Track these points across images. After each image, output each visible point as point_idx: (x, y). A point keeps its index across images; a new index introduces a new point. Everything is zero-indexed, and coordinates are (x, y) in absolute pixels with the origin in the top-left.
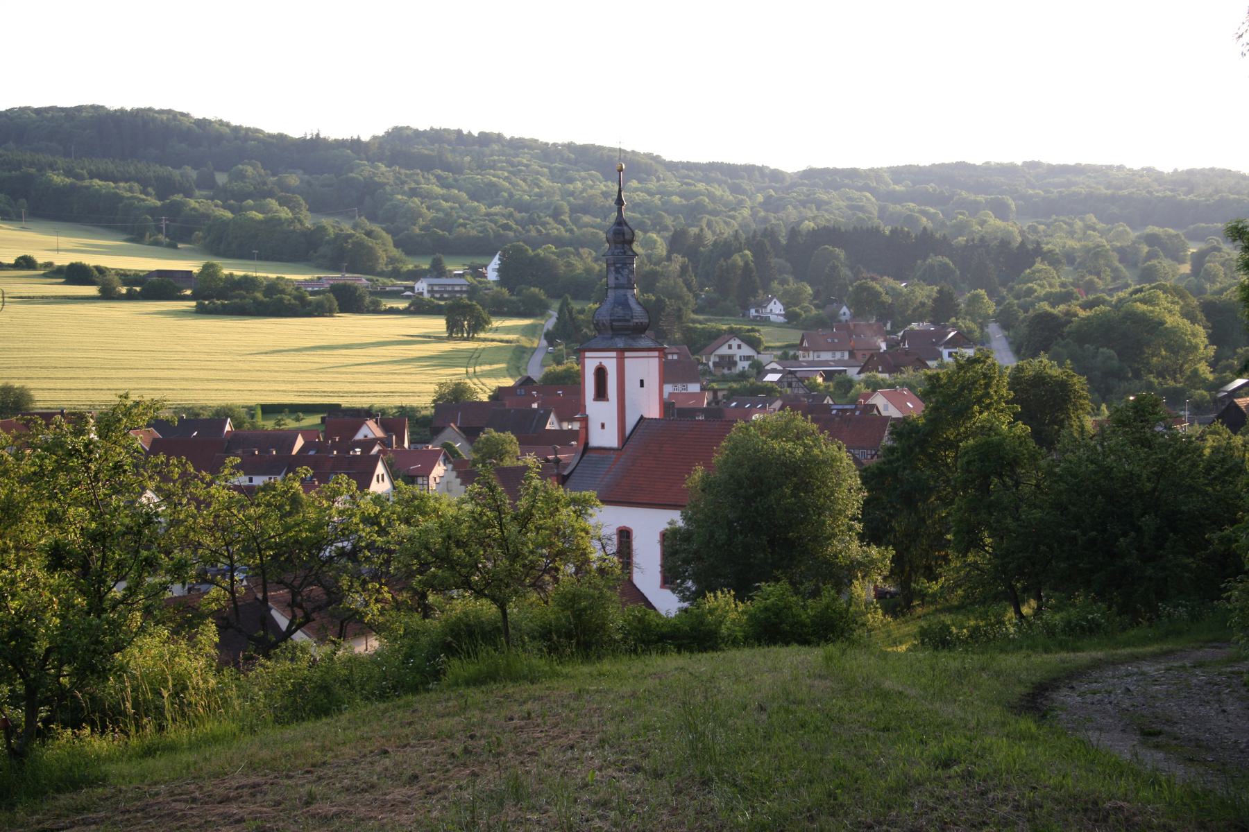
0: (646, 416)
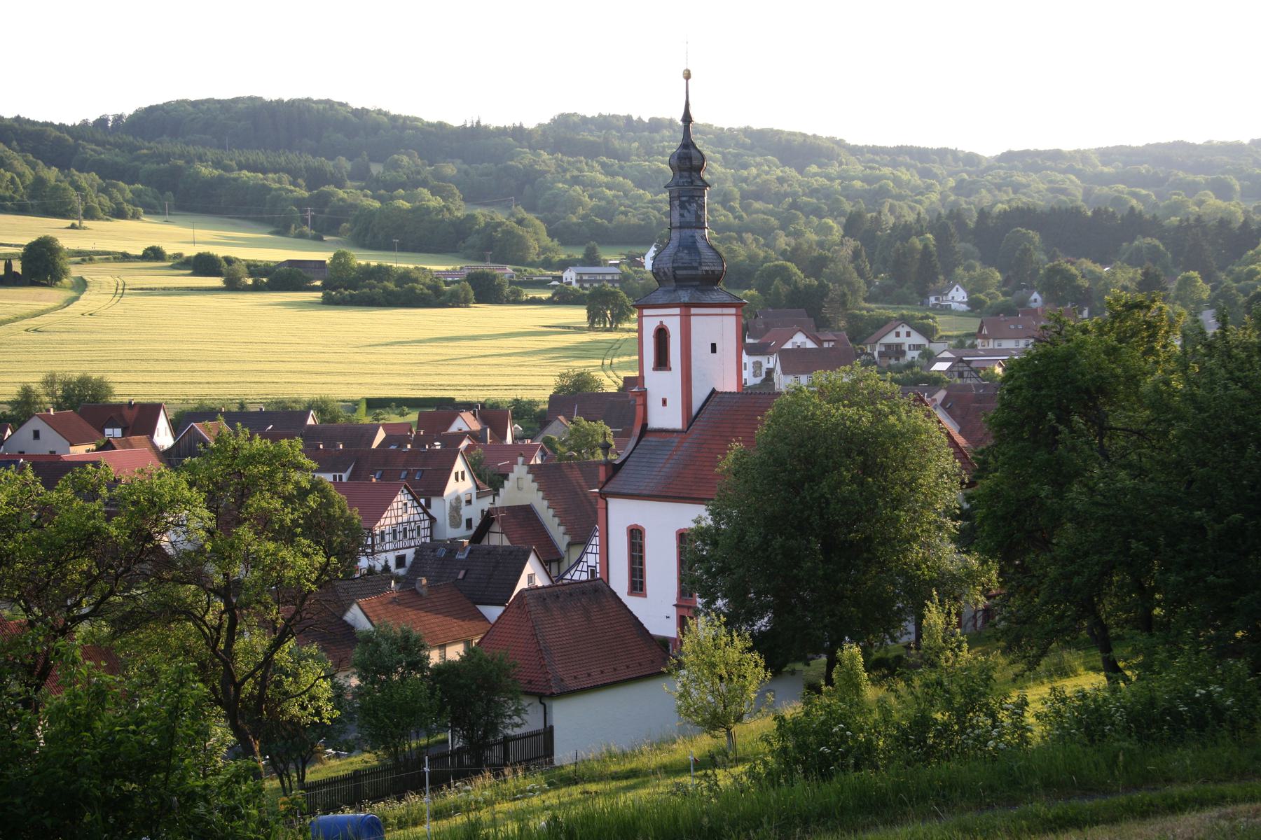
0: (719, 389)
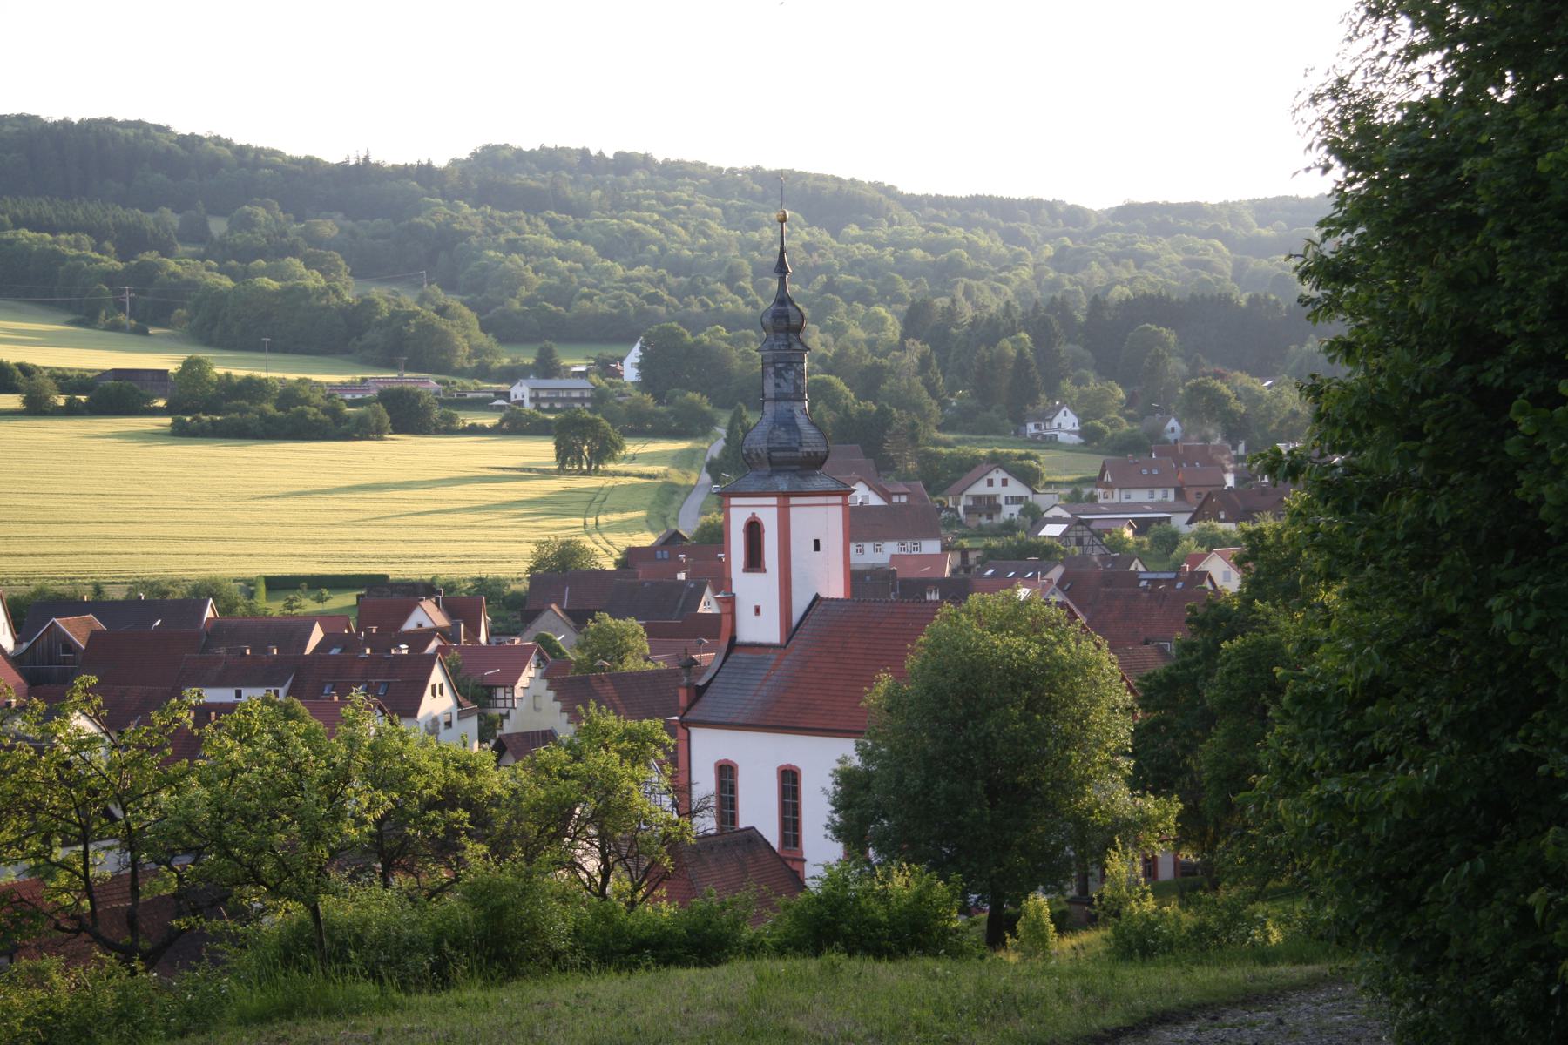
0: (824, 595)
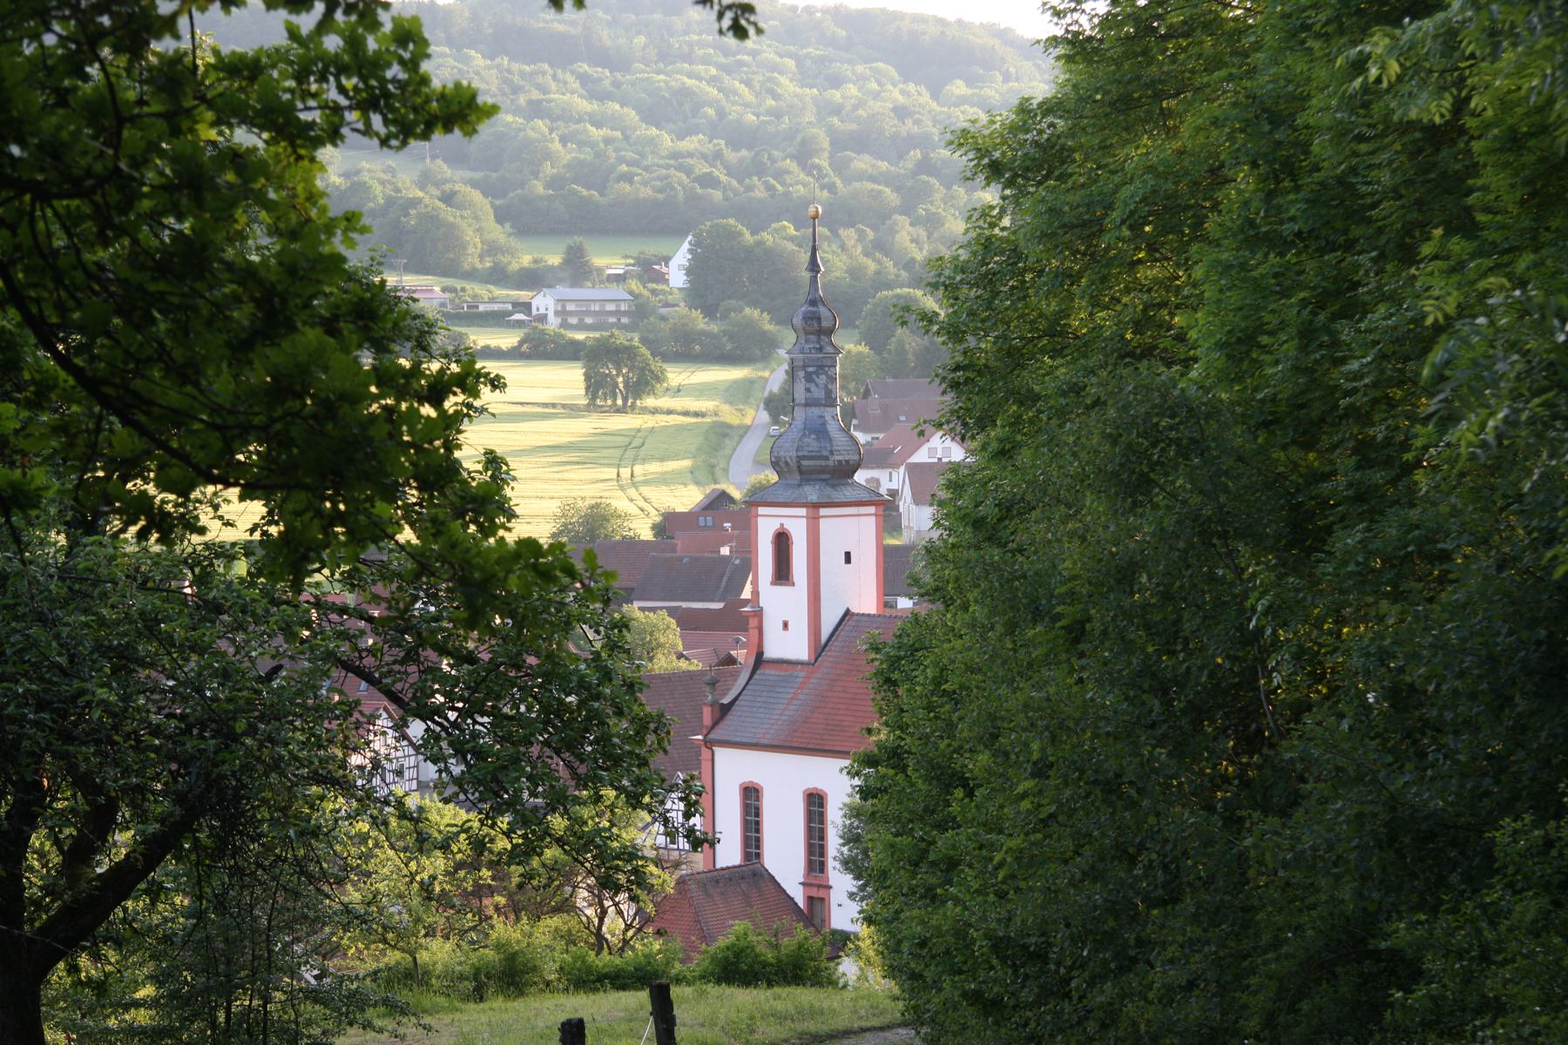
0: (854, 610)
